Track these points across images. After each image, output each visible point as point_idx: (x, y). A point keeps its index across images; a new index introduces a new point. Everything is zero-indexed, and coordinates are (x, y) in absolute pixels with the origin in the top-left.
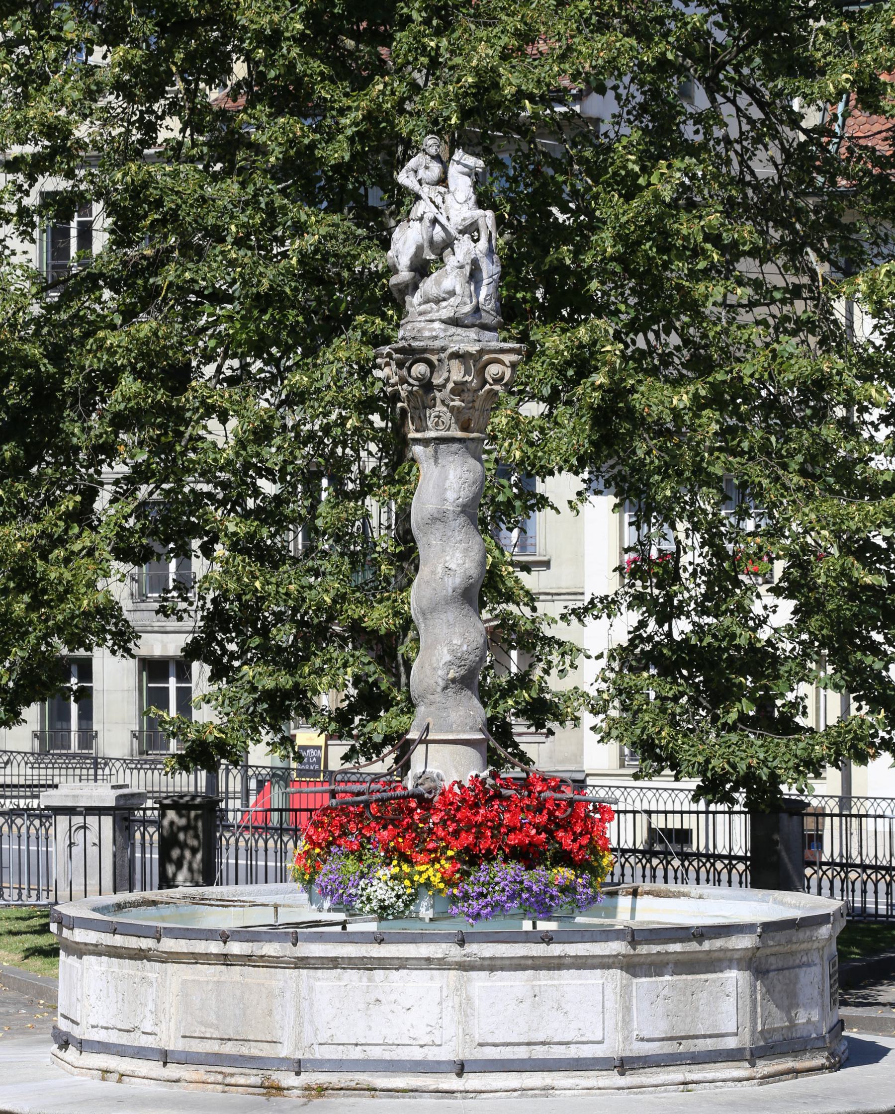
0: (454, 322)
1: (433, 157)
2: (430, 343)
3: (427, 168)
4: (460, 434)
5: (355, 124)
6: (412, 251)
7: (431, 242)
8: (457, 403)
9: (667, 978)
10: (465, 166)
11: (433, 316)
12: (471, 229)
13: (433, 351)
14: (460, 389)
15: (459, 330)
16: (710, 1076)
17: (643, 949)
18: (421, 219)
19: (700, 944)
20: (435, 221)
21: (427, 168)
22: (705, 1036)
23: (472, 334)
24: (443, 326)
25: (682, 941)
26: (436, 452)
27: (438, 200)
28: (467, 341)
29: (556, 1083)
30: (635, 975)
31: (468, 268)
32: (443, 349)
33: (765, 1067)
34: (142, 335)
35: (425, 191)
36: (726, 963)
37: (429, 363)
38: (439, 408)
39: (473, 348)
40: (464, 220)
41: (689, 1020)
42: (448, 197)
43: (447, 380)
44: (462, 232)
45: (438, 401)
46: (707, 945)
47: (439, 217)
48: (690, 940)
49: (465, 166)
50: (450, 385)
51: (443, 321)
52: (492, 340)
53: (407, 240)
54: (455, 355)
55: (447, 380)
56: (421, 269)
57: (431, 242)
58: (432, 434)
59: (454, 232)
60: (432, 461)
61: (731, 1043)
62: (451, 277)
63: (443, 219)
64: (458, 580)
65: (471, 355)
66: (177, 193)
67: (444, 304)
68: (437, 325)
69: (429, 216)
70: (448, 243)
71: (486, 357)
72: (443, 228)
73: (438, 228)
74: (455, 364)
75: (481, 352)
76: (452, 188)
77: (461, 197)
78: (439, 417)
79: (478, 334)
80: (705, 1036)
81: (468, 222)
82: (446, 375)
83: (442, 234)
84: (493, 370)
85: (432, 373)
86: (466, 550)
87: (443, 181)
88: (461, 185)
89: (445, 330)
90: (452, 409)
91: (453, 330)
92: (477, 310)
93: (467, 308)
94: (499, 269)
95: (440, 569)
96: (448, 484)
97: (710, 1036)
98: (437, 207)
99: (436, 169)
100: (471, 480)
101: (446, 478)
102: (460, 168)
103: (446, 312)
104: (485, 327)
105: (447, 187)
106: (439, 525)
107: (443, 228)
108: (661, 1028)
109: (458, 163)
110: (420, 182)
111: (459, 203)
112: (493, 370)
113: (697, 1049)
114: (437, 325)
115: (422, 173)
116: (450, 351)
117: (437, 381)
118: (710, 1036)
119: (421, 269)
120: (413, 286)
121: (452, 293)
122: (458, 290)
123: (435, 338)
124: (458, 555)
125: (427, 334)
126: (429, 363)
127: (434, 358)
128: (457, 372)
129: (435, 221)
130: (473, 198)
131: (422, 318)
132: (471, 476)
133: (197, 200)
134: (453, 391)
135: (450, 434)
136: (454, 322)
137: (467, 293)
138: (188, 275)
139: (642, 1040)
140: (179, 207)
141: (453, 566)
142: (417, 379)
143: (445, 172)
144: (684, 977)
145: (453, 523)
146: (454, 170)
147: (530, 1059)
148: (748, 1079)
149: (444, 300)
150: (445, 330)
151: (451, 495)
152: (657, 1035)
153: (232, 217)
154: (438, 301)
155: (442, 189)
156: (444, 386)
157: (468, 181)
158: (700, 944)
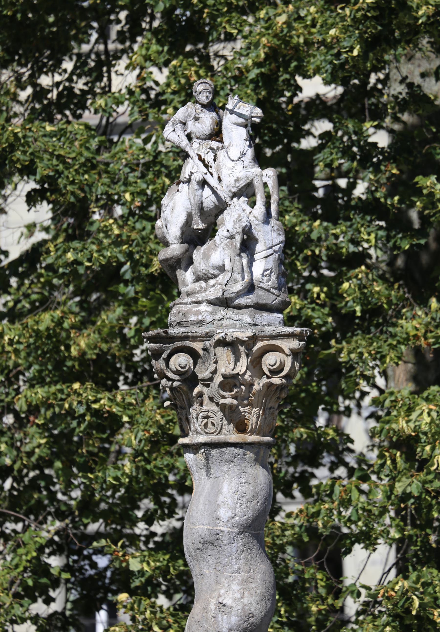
0: (224, 302)
1: (203, 106)
2: (193, 329)
3: (196, 119)
4: (235, 437)
5: (258, 65)
6: (182, 219)
7: (201, 208)
8: (228, 401)
10: (240, 115)
11: (200, 297)
12: (247, 191)
13: (195, 338)
14: (230, 382)
15: (230, 313)
18: (189, 181)
20: (203, 183)
21: (196, 119)
23: (246, 317)
24: (210, 308)
26: (207, 460)
27: (209, 158)
28: (238, 325)
31: (238, 238)
32: (208, 336)
34: (42, 327)
35: (194, 149)
37: (194, 354)
38: (208, 406)
39: (244, 335)
40: (237, 180)
42: (221, 154)
43: (215, 372)
44: (236, 195)
45: (206, 399)
47: (208, 178)
49: (240, 115)
50: (218, 379)
51: (211, 303)
52: (273, 322)
53: (176, 209)
54: (222, 343)
55: (215, 372)
56: (195, 238)
57: (201, 208)
58: (202, 439)
59: (224, 195)
60: (203, 472)
62: (220, 249)
63: (213, 181)
64: (234, 619)
65: (242, 342)
66: (59, 157)
67: (212, 282)
68: (204, 307)
69: (197, 177)
70: (221, 207)
71: (260, 344)
72: (214, 192)
73: (207, 191)
74: (224, 353)
75: (254, 339)
76: (226, 143)
77: (235, 153)
78: (207, 417)
79: (253, 317)
81: (242, 183)
82: (212, 367)
83: (213, 198)
84: (270, 360)
85: (195, 364)
86: (246, 581)
87: (216, 134)
88: (236, 137)
89: (213, 313)
90: (223, 408)
91: (222, 312)
92: (251, 288)
93: (238, 287)
94: (282, 238)
95: (212, 606)
96: (220, 499)
98: (207, 166)
99: (207, 120)
100: (250, 493)
101: (219, 492)
102: (234, 117)
103: (214, 293)
104: (261, 307)
105: (221, 141)
106: (212, 550)
107: (214, 192)
109: (232, 112)
110: (189, 137)
111: (234, 161)
112: (270, 360)
114: (204, 307)
115: (192, 127)
116: (216, 337)
117: (203, 374)
119: (195, 238)
120: (186, 261)
121: (222, 269)
122: (228, 266)
123: (201, 323)
124: (235, 587)
125: (192, 318)
126: (194, 354)
127: (198, 346)
128: (226, 363)
129: (203, 183)
130: (250, 152)
131: (189, 300)
132: (250, 490)
133: (83, 165)
134: (222, 386)
135: (221, 438)
136: (224, 302)
137: (238, 268)
138: (70, 256)
140: (59, 173)
141: (228, 601)
142: (177, 372)
143: (219, 124)
145: (228, 548)
146: (228, 120)
149: (215, 276)
150: (213, 313)
151: (224, 513)
153: (126, 184)
154: (206, 278)
155: (215, 144)
156: (211, 379)
157: (243, 133)
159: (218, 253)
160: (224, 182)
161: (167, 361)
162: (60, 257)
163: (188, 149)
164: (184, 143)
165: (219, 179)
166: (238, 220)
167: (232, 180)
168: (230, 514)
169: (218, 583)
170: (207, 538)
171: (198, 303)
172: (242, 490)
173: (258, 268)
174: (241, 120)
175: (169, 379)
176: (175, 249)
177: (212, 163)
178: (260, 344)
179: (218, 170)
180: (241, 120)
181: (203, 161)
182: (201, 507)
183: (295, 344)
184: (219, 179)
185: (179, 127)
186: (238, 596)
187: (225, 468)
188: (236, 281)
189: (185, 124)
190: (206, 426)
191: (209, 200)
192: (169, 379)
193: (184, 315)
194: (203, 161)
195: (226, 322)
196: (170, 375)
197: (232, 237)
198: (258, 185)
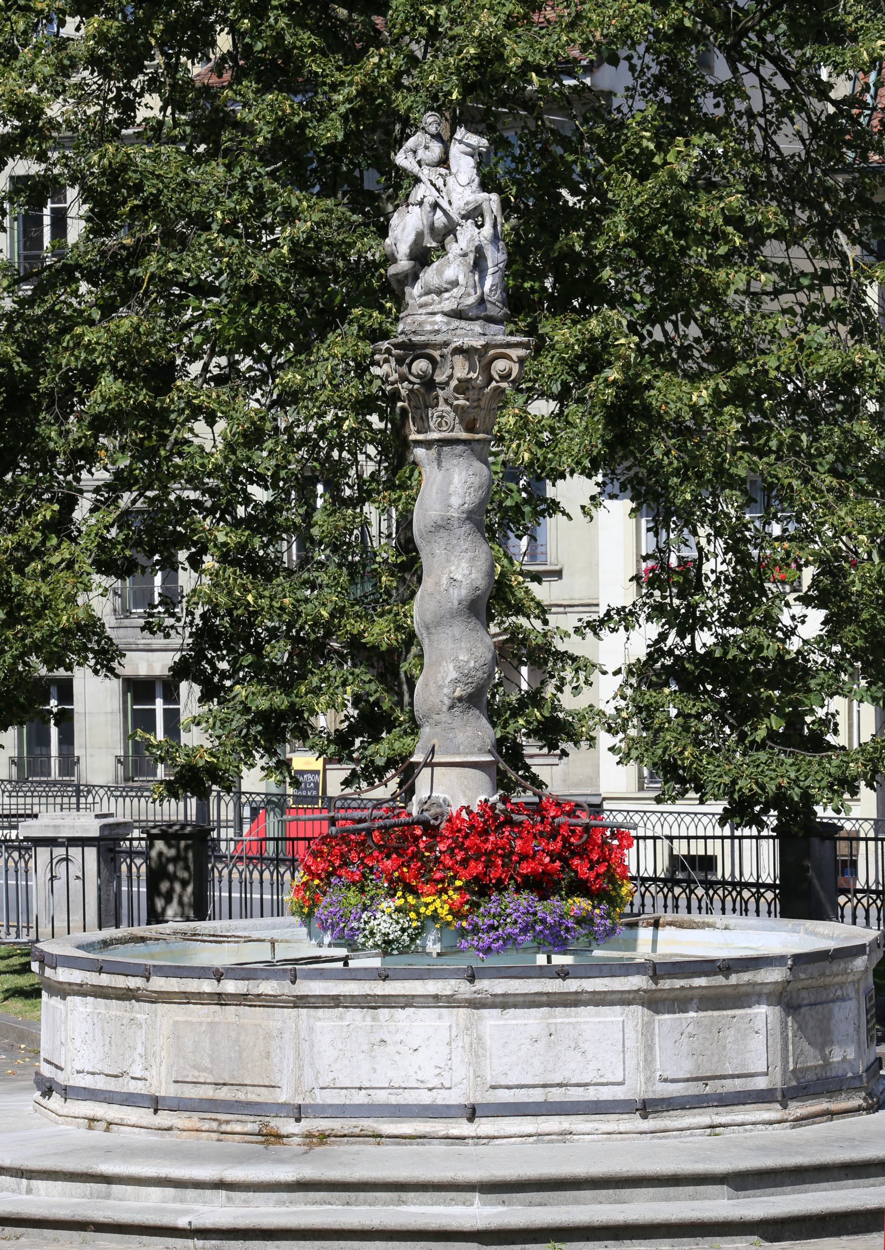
0: (458, 314)
1: (433, 136)
3: (426, 148)
4: (464, 435)
6: (411, 238)
7: (432, 228)
8: (461, 402)
9: (692, 1014)
10: (468, 145)
12: (475, 214)
13: (435, 346)
14: (464, 387)
15: (463, 323)
16: (739, 1118)
17: (666, 984)
18: (421, 204)
19: (727, 978)
20: (436, 206)
21: (426, 148)
22: (733, 1077)
24: (445, 319)
25: (707, 974)
26: (439, 454)
27: (440, 183)
28: (472, 335)
29: (575, 1128)
30: (657, 1012)
31: (472, 256)
32: (446, 344)
33: (797, 1109)
35: (425, 173)
36: (754, 999)
39: (478, 343)
40: (467, 204)
41: (716, 1059)
42: (450, 180)
43: (451, 377)
45: (441, 400)
46: (734, 979)
47: (440, 201)
48: (716, 974)
49: (468, 145)
50: (454, 383)
51: (445, 314)
52: (498, 334)
53: (406, 227)
54: (459, 351)
55: (451, 377)
56: (422, 257)
57: (432, 228)
58: (435, 435)
59: (456, 217)
60: (435, 464)
61: (761, 1083)
63: (444, 204)
64: (464, 592)
68: (439, 318)
69: (429, 200)
70: (450, 230)
71: (492, 352)
73: (439, 213)
74: (459, 359)
75: (487, 347)
76: (453, 170)
77: (464, 178)
78: (442, 417)
79: (483, 327)
80: (733, 1077)
81: (471, 206)
82: (448, 372)
83: (444, 219)
84: (500, 365)
85: (434, 370)
87: (444, 162)
88: (464, 166)
89: (448, 324)
90: (456, 409)
91: (456, 323)
92: (482, 301)
93: (471, 300)
94: (505, 257)
95: (444, 581)
96: (452, 489)
97: (739, 1076)
98: (438, 190)
100: (476, 485)
101: (450, 483)
102: (462, 147)
103: (449, 305)
104: (490, 320)
105: (448, 168)
106: (443, 533)
108: (686, 1069)
109: (461, 142)
110: (419, 163)
113: (725, 1090)
114: (439, 318)
116: (453, 345)
117: (440, 378)
118: (739, 1076)
119: (422, 257)
120: (413, 277)
121: (455, 284)
122: (462, 280)
123: (437, 332)
124: (464, 565)
125: (428, 327)
127: (436, 354)
128: (461, 369)
129: (436, 206)
130: (477, 180)
131: (423, 311)
132: (476, 480)
134: (457, 390)
136: (458, 314)
137: (471, 283)
139: (666, 1080)
141: (458, 577)
142: (418, 376)
144: (710, 1013)
146: (455, 149)
147: (546, 1102)
148: (779, 1122)
149: (447, 290)
151: (455, 501)
152: (681, 1075)
154: (439, 292)
155: (443, 171)
156: (447, 383)
157: (471, 162)
158: (727, 978)
159: (451, 268)
160: (454, 205)
161: (410, 366)
162: (161, 267)
163: (420, 175)
164: (416, 169)
165: (450, 203)
166: (472, 239)
167: (462, 204)
168: (460, 502)
169: (448, 561)
170: (439, 522)
171: (434, 314)
172: (470, 480)
173: (489, 282)
174: (469, 150)
175: (410, 382)
176: (403, 264)
177: (442, 188)
178: (492, 352)
179: (448, 194)
180: (469, 150)
181: (434, 185)
182: (434, 495)
183: (522, 352)
184: (450, 203)
185: (410, 154)
186: (467, 572)
187: (455, 462)
188: (469, 295)
189: (415, 152)
190: (440, 425)
191: (439, 218)
192: (410, 382)
193: (420, 324)
194: (434, 185)
195: (459, 332)
196: (412, 378)
197: (465, 255)
198: (485, 206)
